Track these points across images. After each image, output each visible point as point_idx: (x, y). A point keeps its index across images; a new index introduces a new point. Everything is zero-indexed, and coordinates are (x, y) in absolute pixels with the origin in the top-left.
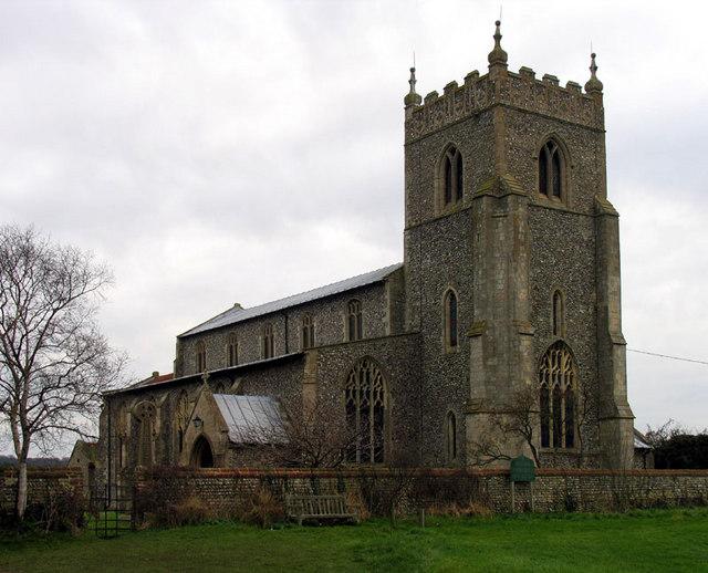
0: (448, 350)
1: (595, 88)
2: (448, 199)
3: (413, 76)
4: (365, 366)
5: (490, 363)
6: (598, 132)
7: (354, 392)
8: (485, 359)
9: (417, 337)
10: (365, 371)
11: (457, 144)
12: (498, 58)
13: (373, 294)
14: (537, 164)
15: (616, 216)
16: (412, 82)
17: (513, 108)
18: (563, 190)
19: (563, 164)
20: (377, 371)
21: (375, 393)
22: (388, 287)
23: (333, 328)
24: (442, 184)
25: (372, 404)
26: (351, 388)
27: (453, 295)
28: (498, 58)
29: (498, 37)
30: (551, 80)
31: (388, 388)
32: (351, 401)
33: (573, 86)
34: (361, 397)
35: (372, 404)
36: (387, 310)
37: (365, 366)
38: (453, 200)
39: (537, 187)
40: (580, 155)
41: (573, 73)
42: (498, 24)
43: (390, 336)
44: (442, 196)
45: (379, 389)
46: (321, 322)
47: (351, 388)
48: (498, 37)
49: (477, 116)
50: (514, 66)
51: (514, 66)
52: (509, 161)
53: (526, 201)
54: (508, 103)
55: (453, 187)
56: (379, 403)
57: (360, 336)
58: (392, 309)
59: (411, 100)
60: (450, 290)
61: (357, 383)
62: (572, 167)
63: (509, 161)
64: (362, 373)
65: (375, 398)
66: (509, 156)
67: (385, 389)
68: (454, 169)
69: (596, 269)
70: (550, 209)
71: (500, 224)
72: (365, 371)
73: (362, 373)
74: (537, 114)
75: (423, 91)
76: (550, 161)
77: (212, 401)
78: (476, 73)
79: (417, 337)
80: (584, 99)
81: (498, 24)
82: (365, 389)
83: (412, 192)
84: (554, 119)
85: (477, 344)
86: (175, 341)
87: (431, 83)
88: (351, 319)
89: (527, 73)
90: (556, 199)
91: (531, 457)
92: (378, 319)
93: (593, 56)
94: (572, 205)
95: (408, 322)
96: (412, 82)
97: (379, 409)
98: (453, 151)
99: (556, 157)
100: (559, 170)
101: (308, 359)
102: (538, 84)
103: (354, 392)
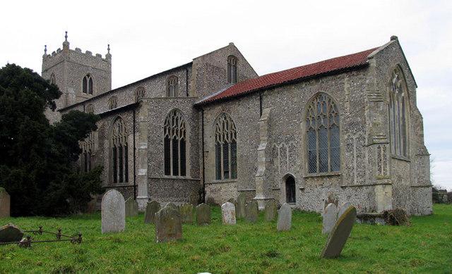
1: (109, 56)
12: (66, 45)
16: (45, 50)
28: (66, 45)
51: (72, 47)
89: (78, 50)
96: (45, 50)
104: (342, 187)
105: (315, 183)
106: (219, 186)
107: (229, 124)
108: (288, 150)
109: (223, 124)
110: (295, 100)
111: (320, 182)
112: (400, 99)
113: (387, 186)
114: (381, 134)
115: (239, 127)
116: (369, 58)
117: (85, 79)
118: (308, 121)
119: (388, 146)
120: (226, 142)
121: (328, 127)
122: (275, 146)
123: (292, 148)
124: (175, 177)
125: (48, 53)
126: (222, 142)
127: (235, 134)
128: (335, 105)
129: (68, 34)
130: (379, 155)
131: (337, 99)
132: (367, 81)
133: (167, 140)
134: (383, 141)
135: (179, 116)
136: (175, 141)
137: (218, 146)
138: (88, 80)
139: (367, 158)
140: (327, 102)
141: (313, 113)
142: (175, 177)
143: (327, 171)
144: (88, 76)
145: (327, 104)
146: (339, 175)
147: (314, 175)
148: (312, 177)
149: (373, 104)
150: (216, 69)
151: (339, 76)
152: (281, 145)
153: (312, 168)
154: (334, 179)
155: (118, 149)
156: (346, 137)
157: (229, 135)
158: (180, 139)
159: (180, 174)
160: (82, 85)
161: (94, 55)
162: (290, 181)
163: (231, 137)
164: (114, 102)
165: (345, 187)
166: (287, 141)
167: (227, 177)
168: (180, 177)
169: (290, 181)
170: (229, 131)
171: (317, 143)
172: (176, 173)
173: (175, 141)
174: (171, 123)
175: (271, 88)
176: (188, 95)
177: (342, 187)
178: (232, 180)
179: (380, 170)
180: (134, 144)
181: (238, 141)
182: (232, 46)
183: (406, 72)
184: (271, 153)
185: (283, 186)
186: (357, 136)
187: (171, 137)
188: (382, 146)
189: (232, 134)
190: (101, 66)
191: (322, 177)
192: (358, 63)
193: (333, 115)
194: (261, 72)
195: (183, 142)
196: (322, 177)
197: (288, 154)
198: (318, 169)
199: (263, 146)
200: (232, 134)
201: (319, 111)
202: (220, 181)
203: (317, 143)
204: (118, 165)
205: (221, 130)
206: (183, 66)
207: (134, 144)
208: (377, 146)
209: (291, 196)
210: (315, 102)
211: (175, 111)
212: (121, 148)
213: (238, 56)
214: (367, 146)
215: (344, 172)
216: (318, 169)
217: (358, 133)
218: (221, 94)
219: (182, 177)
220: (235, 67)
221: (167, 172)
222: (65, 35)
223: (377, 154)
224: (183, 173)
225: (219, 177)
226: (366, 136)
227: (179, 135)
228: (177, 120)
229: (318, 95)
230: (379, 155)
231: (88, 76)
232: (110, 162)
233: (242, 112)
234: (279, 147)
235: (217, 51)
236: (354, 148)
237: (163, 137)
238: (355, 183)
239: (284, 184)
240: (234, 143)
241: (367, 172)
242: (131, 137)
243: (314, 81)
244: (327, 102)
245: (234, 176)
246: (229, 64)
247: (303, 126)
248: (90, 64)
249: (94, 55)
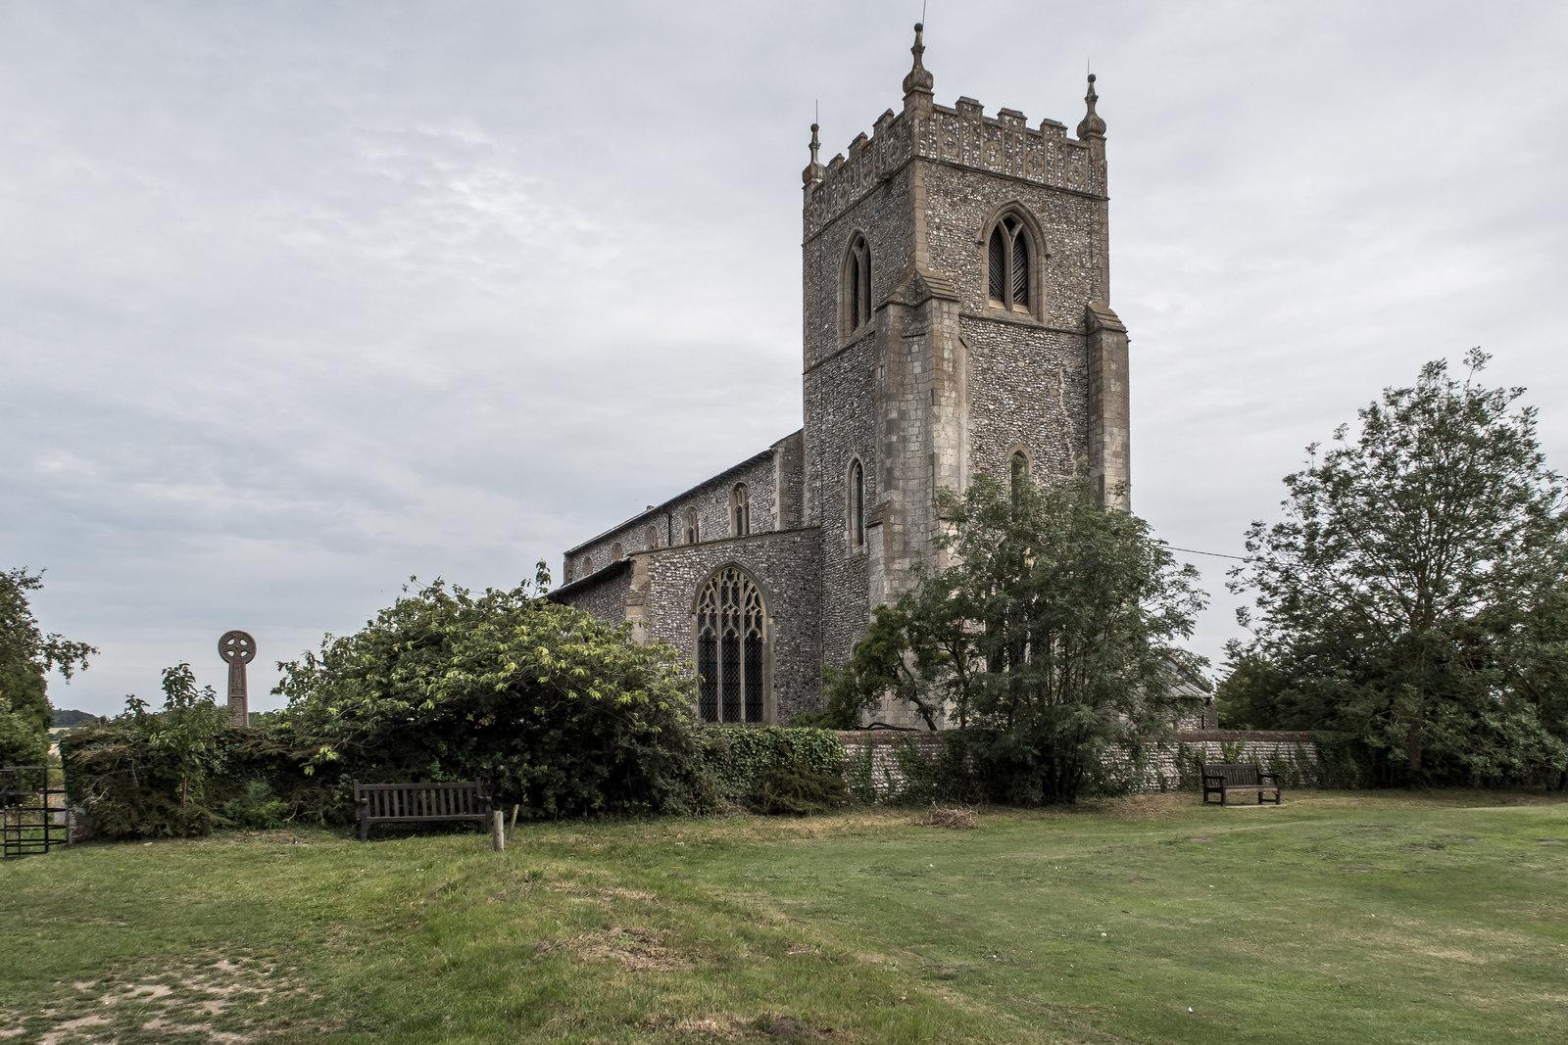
0: (855, 551)
1: (1093, 130)
2: (855, 323)
3: (815, 137)
4: (730, 577)
5: (896, 566)
6: (1091, 200)
8: (890, 560)
9: (817, 532)
10: (730, 585)
11: (865, 231)
12: (917, 85)
13: (760, 473)
14: (985, 252)
17: (943, 163)
18: (1033, 293)
19: (1032, 253)
20: (751, 586)
21: (748, 619)
22: (777, 461)
23: (717, 520)
24: (849, 298)
25: (742, 635)
26: (708, 612)
27: (859, 466)
29: (918, 50)
31: (768, 612)
32: (708, 632)
34: (725, 624)
35: (742, 635)
36: (776, 496)
37: (730, 577)
38: (862, 324)
39: (985, 288)
40: (1059, 237)
42: (919, 28)
43: (779, 532)
44: (848, 316)
45: (753, 613)
46: (706, 519)
47: (708, 612)
48: (918, 50)
49: (886, 180)
50: (945, 96)
51: (945, 96)
52: (949, 231)
53: (956, 309)
54: (933, 155)
55: (861, 304)
57: (748, 531)
58: (782, 494)
59: (808, 175)
60: (856, 460)
61: (718, 603)
62: (1048, 256)
63: (949, 231)
64: (725, 590)
65: (748, 625)
66: (944, 235)
67: (764, 612)
68: (860, 273)
69: (1088, 417)
70: (1007, 324)
71: (915, 348)
72: (730, 585)
73: (725, 590)
74: (987, 173)
76: (1012, 249)
78: (889, 113)
79: (817, 532)
80: (1072, 145)
81: (919, 28)
82: (730, 613)
83: (811, 316)
84: (1017, 180)
85: (877, 535)
86: (563, 559)
87: (836, 145)
88: (799, 511)
89: (968, 107)
90: (1017, 308)
92: (768, 508)
93: (1092, 79)
94: (1046, 317)
95: (807, 512)
97: (754, 643)
98: (862, 243)
99: (1021, 239)
100: (1026, 265)
101: (636, 568)
102: (988, 125)
103: (713, 617)
117: (997, 238)
173: (730, 643)
212: (730, 643)
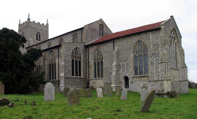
1: (47, 24)
7: (77, 57)
12: (29, 19)
15: (6, 28)
16: (20, 22)
23: (69, 39)
28: (29, 19)
29: (29, 16)
30: (39, 23)
33: (43, 24)
41: (43, 21)
51: (31, 21)
52: (172, 17)
56: (76, 60)
75: (22, 23)
77: (19, 31)
89: (34, 22)
91: (111, 86)
96: (20, 22)
103: (77, 57)
104: (149, 81)
105: (137, 79)
106: (95, 81)
107: (100, 54)
108: (125, 65)
109: (97, 54)
110: (129, 43)
111: (140, 79)
112: (174, 43)
113: (169, 81)
114: (166, 58)
115: (104, 55)
116: (161, 25)
117: (37, 35)
118: (134, 52)
119: (169, 63)
120: (98, 62)
121: (143, 55)
122: (120, 63)
123: (127, 64)
124: (76, 77)
125: (21, 23)
126: (97, 62)
127: (103, 58)
128: (146, 46)
129: (30, 15)
130: (165, 67)
131: (147, 43)
132: (160, 35)
133: (73, 61)
134: (167, 61)
135: (78, 51)
136: (76, 61)
137: (95, 63)
138: (38, 35)
139: (160, 69)
140: (142, 44)
141: (136, 49)
142: (76, 77)
143: (142, 74)
144: (38, 33)
145: (143, 45)
146: (148, 76)
147: (137, 76)
148: (136, 77)
149: (162, 45)
150: (94, 30)
151: (148, 33)
152: (122, 63)
153: (136, 73)
154: (145, 78)
155: (51, 65)
156: (151, 60)
157: (100, 59)
158: (78, 61)
159: (78, 76)
160: (36, 37)
161: (41, 24)
162: (126, 79)
163: (101, 60)
164: (50, 44)
165: (151, 81)
166: (125, 61)
167: (99, 77)
168: (78, 77)
169: (126, 79)
170: (100, 57)
171: (138, 62)
172: (77, 75)
173: (76, 61)
174: (75, 53)
175: (118, 38)
176: (82, 41)
177: (149, 81)
178: (101, 78)
179: (166, 74)
180: (59, 63)
181: (104, 61)
182: (101, 20)
183: (177, 31)
184: (118, 66)
185: (123, 81)
186: (156, 59)
187: (75, 60)
188: (166, 64)
189: (101, 58)
190: (44, 28)
191: (140, 77)
192: (156, 27)
193: (145, 50)
194: (114, 31)
195: (80, 62)
196: (140, 77)
197: (125, 67)
198: (138, 73)
199: (114, 64)
200: (101, 58)
201: (139, 48)
202: (96, 79)
203: (138, 62)
204: (52, 72)
205: (96, 57)
206: (80, 29)
207: (59, 63)
208: (164, 63)
209: (127, 85)
210: (137, 44)
211: (76, 48)
212: (53, 64)
213: (104, 24)
214: (160, 63)
215: (150, 75)
216: (138, 73)
217: (156, 58)
218: (96, 41)
219: (79, 77)
220: (103, 29)
221: (73, 75)
222: (28, 15)
223: (164, 67)
224: (80, 75)
225: (95, 77)
226: (160, 59)
227: (78, 58)
228: (77, 52)
229: (139, 41)
230: (165, 67)
231: (38, 33)
232: (48, 71)
233: (105, 49)
234: (122, 64)
235: (94, 22)
236: (155, 64)
237: (71, 60)
238: (155, 80)
239: (124, 80)
240: (102, 62)
241: (160, 75)
242: (57, 60)
243: (137, 35)
244: (142, 44)
245: (102, 77)
246: (100, 28)
247: (132, 55)
248: (39, 28)
249: (41, 24)
